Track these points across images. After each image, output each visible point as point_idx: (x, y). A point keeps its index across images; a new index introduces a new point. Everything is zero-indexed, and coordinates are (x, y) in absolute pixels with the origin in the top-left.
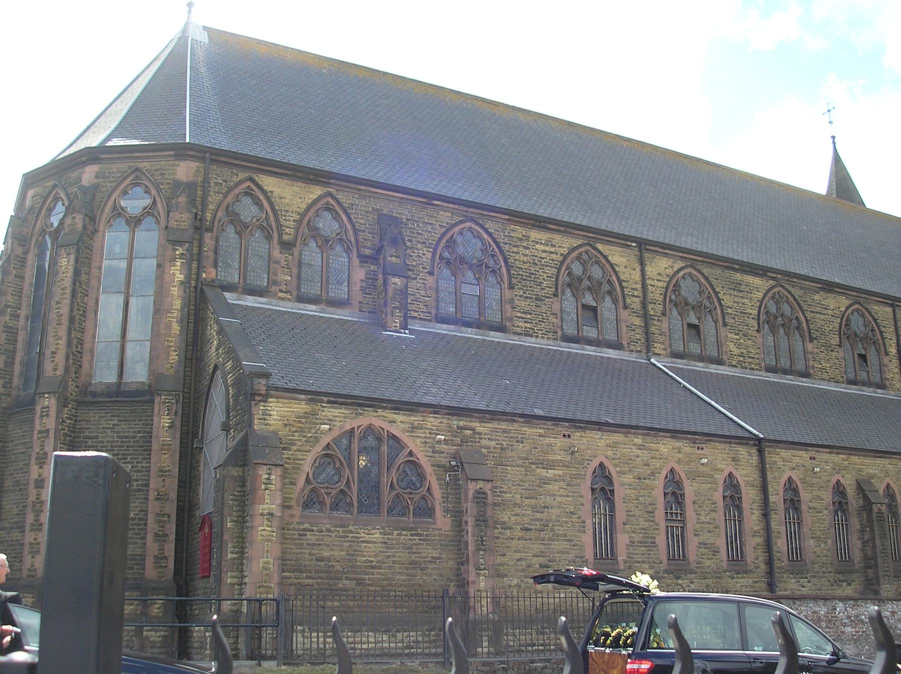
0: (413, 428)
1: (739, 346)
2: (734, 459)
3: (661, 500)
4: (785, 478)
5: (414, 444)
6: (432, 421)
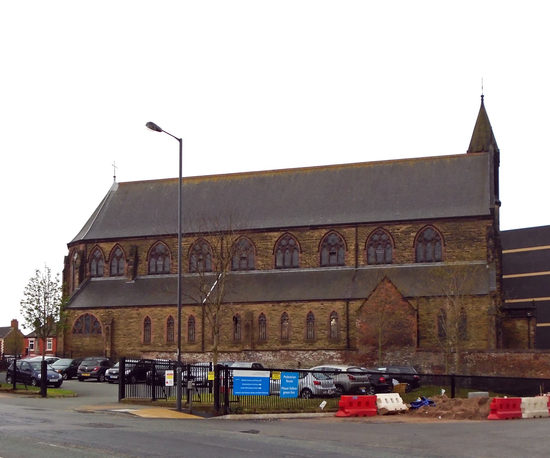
0: (97, 313)
1: (262, 261)
5: (97, 316)
6: (102, 311)
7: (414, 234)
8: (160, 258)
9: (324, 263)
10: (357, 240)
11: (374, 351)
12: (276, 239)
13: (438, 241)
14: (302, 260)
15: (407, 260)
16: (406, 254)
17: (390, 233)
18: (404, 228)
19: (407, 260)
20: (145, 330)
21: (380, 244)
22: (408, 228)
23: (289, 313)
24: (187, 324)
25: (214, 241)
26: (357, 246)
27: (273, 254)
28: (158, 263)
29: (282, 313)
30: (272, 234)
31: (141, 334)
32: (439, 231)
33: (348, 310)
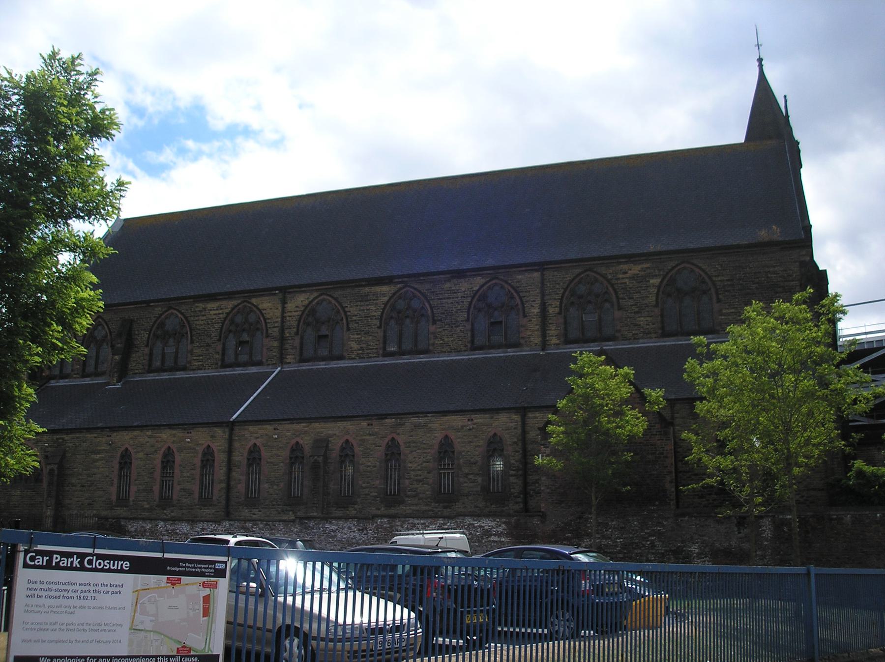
1: (359, 342)
2: (212, 437)
3: (160, 465)
4: (251, 444)
7: (655, 281)
8: (171, 340)
9: (477, 343)
10: (543, 295)
11: (580, 518)
12: (386, 299)
13: (704, 292)
14: (436, 338)
15: (644, 333)
16: (642, 320)
17: (608, 281)
18: (635, 269)
19: (644, 333)
20: (120, 476)
21: (590, 302)
22: (642, 270)
23: (401, 439)
24: (199, 464)
25: (268, 306)
26: (544, 307)
27: (380, 327)
28: (168, 350)
29: (386, 440)
30: (378, 289)
31: (112, 485)
32: (706, 273)
33: (524, 432)
